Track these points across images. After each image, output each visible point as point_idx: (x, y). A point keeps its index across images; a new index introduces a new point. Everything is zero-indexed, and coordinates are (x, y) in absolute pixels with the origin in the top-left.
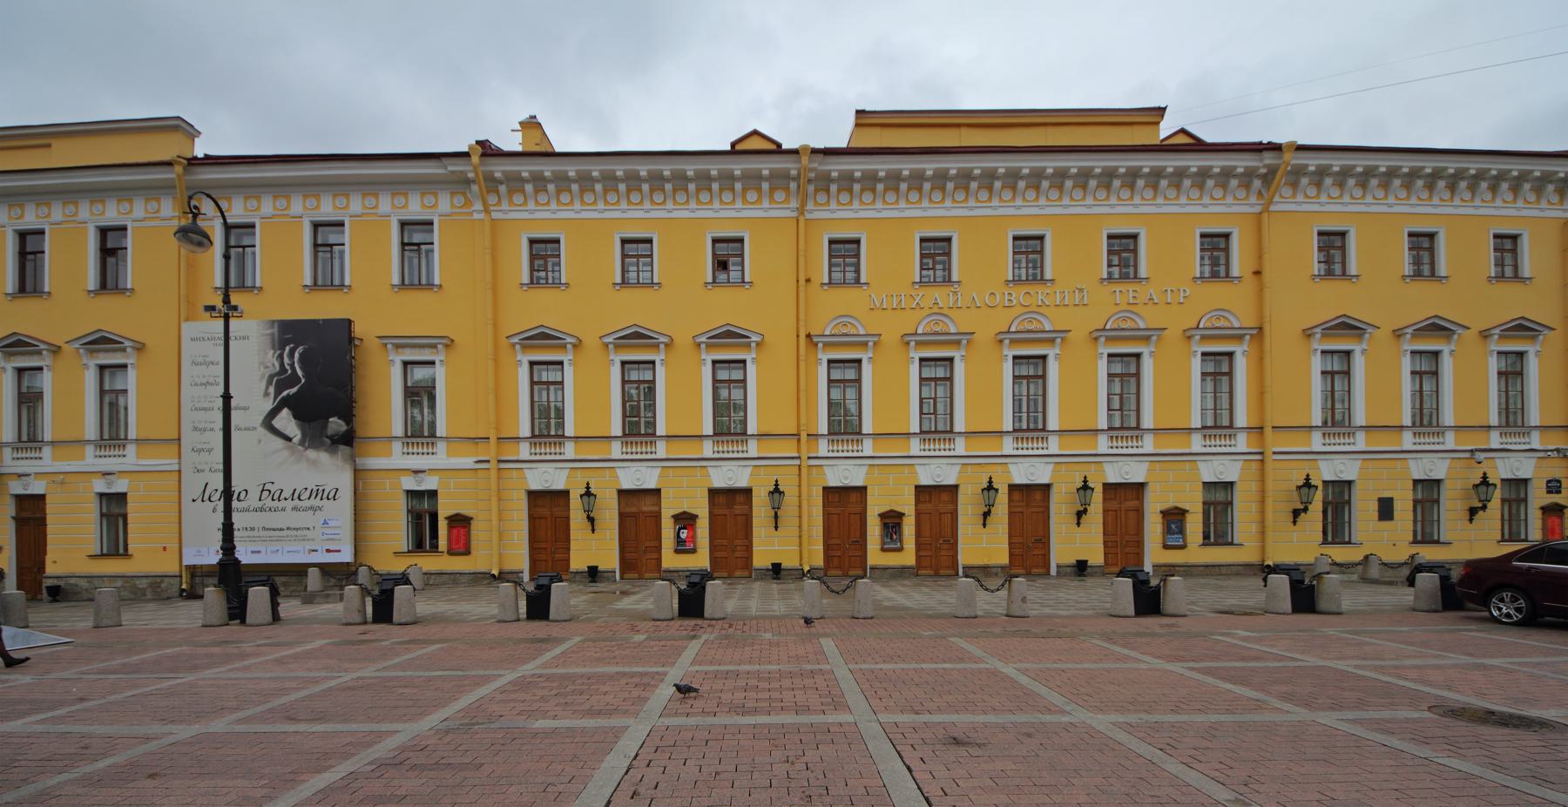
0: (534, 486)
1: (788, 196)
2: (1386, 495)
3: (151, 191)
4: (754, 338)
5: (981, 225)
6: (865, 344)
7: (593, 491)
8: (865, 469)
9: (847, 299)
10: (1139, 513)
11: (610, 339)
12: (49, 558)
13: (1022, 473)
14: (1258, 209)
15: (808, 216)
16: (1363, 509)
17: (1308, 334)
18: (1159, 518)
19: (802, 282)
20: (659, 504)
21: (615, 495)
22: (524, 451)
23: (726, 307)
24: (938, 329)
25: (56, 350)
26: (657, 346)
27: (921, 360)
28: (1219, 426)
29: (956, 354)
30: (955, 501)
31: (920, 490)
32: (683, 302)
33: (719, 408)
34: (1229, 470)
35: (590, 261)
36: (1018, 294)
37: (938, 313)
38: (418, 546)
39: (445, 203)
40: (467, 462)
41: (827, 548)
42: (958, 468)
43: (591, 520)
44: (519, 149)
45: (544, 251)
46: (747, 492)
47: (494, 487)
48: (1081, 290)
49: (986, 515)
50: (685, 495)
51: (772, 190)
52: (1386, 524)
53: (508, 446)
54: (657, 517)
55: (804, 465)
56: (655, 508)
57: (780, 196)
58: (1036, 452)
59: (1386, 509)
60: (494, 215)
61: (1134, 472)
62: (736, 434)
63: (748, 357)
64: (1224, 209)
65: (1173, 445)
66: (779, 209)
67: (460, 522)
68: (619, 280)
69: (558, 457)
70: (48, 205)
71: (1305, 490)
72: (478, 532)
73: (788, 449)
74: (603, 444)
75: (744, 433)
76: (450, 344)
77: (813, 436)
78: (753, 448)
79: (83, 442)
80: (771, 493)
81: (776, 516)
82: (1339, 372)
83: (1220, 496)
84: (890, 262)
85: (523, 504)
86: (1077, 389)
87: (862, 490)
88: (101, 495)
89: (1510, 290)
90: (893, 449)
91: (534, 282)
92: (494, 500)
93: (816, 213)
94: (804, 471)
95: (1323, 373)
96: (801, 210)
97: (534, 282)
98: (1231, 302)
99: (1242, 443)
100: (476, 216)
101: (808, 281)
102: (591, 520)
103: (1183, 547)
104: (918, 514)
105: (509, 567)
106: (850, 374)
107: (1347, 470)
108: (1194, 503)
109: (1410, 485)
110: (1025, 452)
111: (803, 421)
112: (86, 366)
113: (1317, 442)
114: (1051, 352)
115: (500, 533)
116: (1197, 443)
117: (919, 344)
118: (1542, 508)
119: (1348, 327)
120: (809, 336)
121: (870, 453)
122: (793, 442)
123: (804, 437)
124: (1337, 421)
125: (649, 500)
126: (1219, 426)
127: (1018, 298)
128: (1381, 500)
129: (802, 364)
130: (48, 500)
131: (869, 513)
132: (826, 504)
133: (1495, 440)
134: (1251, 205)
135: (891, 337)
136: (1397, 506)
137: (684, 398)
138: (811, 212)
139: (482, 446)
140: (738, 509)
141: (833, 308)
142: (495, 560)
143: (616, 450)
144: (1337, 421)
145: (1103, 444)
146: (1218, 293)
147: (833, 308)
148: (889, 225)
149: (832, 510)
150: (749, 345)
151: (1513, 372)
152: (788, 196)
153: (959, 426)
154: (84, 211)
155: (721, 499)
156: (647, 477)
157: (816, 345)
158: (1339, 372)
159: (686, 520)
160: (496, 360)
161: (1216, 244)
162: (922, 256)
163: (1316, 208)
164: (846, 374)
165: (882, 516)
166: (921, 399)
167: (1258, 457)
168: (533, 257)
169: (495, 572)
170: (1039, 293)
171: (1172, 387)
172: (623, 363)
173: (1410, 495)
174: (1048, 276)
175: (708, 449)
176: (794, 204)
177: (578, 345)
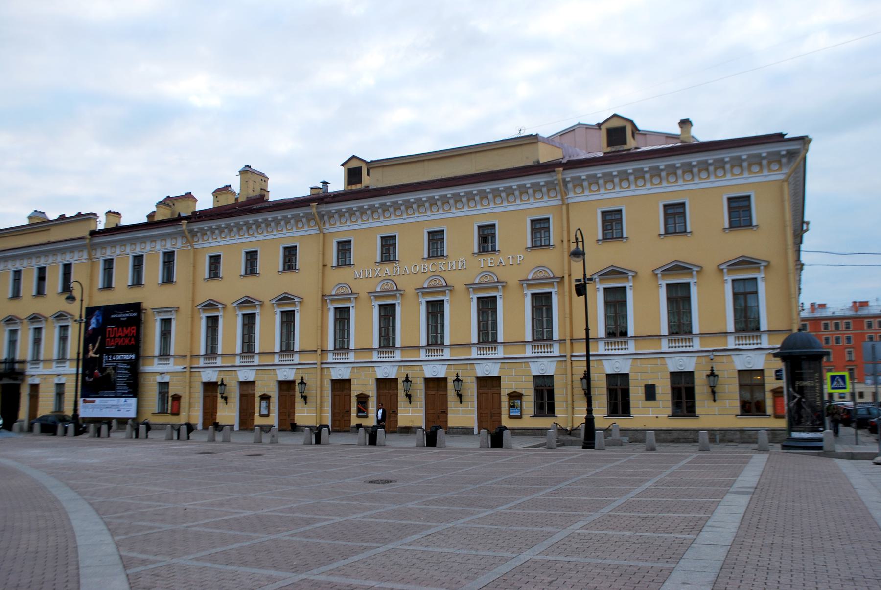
0: (281, 379)
2: (650, 382)
3: (80, 248)
5: (411, 227)
6: (552, 283)
8: (217, 373)
13: (483, 370)
14: (560, 203)
23: (743, 244)
25: (46, 319)
26: (255, 306)
31: (380, 381)
36: (429, 266)
38: (163, 411)
39: (179, 243)
40: (179, 368)
47: (188, 381)
50: (518, 381)
53: (195, 360)
54: (254, 395)
55: (323, 367)
58: (435, 358)
59: (650, 393)
60: (196, 247)
61: (493, 370)
64: (541, 205)
67: (177, 398)
68: (662, 232)
70: (135, 244)
71: (712, 378)
72: (184, 403)
74: (231, 358)
76: (177, 309)
80: (708, 376)
84: (365, 251)
88: (160, 383)
90: (267, 361)
91: (605, 238)
92: (188, 388)
93: (329, 229)
97: (605, 238)
99: (556, 350)
102: (460, 396)
103: (520, 417)
105: (324, 423)
112: (55, 327)
115: (190, 404)
117: (529, 286)
121: (634, 352)
132: (427, 388)
133: (731, 343)
136: (659, 391)
142: (570, 423)
146: (543, 257)
148: (364, 231)
149: (337, 393)
150: (294, 303)
154: (128, 249)
155: (431, 385)
159: (515, 396)
160: (193, 318)
163: (599, 197)
165: (358, 396)
169: (569, 429)
170: (440, 264)
176: (559, 197)
177: (636, 275)
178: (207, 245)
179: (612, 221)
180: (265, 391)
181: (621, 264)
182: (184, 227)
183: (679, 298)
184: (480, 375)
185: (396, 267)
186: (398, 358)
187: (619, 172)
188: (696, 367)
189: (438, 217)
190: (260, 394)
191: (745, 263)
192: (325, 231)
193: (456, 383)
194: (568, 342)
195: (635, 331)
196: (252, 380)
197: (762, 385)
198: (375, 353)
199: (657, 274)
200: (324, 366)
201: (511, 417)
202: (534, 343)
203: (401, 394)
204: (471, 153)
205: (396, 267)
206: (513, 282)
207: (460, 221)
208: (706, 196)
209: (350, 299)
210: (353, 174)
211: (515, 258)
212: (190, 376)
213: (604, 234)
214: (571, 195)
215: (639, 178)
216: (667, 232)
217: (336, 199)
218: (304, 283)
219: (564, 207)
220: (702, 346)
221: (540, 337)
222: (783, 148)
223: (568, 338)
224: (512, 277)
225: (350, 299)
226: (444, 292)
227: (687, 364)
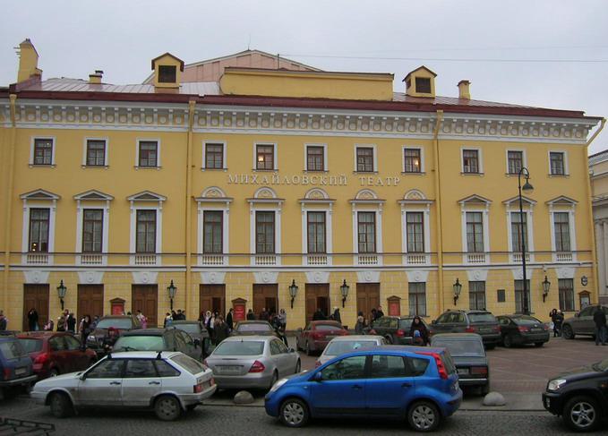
1: (21, 117)
4: (161, 199)
5: (291, 139)
7: (64, 285)
8: (379, 273)
9: (214, 177)
10: (378, 298)
11: (24, 197)
13: (363, 277)
14: (433, 137)
15: (194, 131)
16: (491, 296)
17: (459, 203)
18: (110, 304)
19: (190, 167)
23: (147, 181)
27: (407, 213)
28: (416, 251)
29: (377, 211)
32: (121, 178)
33: (87, 236)
34: (422, 276)
35: (70, 153)
36: (310, 177)
37: (266, 187)
42: (102, 274)
44: (217, 94)
45: (43, 148)
46: (155, 286)
48: (343, 177)
49: (545, 296)
50: (118, 289)
51: (174, 117)
52: (502, 304)
57: (178, 120)
59: (501, 296)
61: (373, 277)
64: (415, 137)
66: (178, 128)
68: (32, 162)
69: (43, 265)
71: (172, 290)
73: (179, 262)
77: (195, 255)
79: (301, 255)
81: (62, 302)
82: (475, 225)
83: (567, 285)
85: (21, 292)
86: (342, 232)
89: (558, 181)
93: (197, 129)
95: (467, 223)
96: (191, 128)
98: (420, 186)
99: (428, 261)
100: (6, 126)
101: (193, 166)
106: (319, 219)
107: (481, 275)
109: (407, 285)
110: (414, 265)
111: (189, 246)
113: (465, 261)
114: (328, 210)
116: (405, 262)
118: (111, 301)
119: (477, 200)
120: (193, 197)
121: (228, 265)
122: (182, 258)
123: (189, 255)
124: (475, 249)
126: (416, 251)
128: (498, 291)
129: (189, 216)
131: (381, 297)
134: (429, 136)
135: (391, 201)
136: (495, 295)
137: (119, 230)
138: (196, 129)
140: (149, 297)
141: (209, 183)
143: (78, 261)
144: (475, 249)
145: (356, 262)
146: (414, 180)
147: (209, 183)
151: (562, 224)
152: (21, 117)
153: (379, 250)
156: (94, 277)
157: (197, 202)
158: (475, 225)
161: (412, 154)
162: (358, 156)
164: (214, 221)
167: (590, 265)
168: (36, 148)
170: (321, 177)
171: (391, 231)
172: (84, 210)
173: (513, 288)
174: (481, 171)
175: (132, 261)
178: (204, 131)
179: (43, 149)
180: (117, 295)
181: (152, 189)
182: (13, 102)
183: (317, 223)
184: (83, 282)
185: (275, 176)
186: (278, 265)
187: (41, 107)
189: (332, 134)
190: (386, 297)
191: (94, 196)
192: (439, 138)
194: (440, 254)
195: (577, 245)
204: (278, 76)
205: (275, 176)
206: (391, 201)
207: (341, 141)
208: (493, 144)
209: (378, 204)
210: (167, 71)
211: (389, 177)
213: (88, 161)
214: (195, 126)
215: (253, 119)
216: (35, 163)
217: (94, 97)
218: (166, 180)
219: (436, 142)
220: (162, 262)
221: (89, 249)
222: (577, 123)
224: (342, 196)
225: (278, 203)
226: (378, 204)
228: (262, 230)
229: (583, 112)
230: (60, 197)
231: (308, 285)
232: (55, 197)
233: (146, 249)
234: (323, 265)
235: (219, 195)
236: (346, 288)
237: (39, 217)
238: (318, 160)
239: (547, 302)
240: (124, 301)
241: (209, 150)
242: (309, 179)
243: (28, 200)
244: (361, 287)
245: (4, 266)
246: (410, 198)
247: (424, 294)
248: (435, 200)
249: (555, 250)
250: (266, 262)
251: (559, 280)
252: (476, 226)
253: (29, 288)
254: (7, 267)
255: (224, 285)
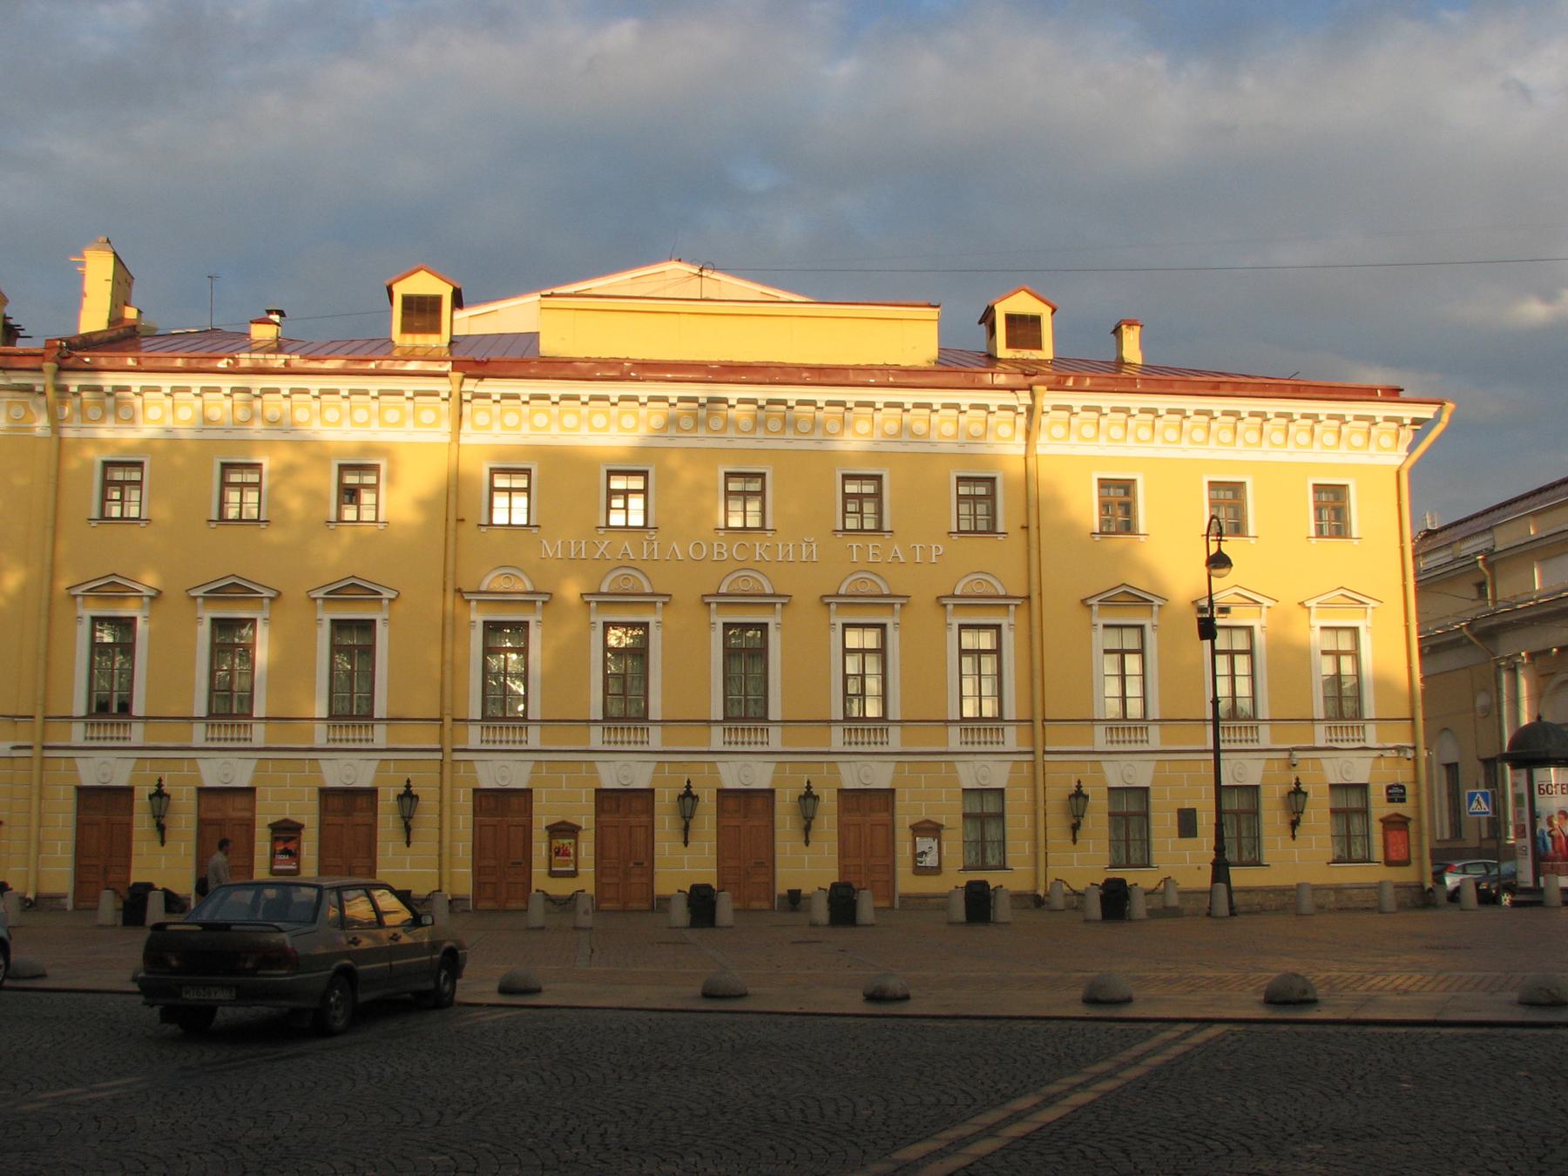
11: (78, 591)
12: (135, 863)
13: (736, 774)
16: (1163, 822)
20: (252, 809)
21: (194, 795)
22: (78, 733)
24: (629, 587)
30: (650, 810)
31: (327, 795)
34: (996, 774)
41: (478, 871)
42: (1008, 766)
43: (161, 828)
46: (372, 793)
54: (249, 825)
55: (447, 756)
56: (247, 814)
59: (1187, 823)
61: (879, 775)
62: (358, 717)
63: (379, 617)
65: (925, 741)
69: (364, 745)
73: (425, 737)
74: (181, 727)
75: (370, 716)
78: (380, 735)
80: (400, 797)
87: (526, 793)
90: (170, 735)
94: (447, 768)
99: (1012, 738)
102: (161, 828)
104: (323, 826)
105: (50, 888)
108: (950, 814)
115: (39, 843)
120: (459, 591)
122: (434, 729)
123: (448, 720)
125: (240, 802)
127: (729, 550)
130: (1152, 793)
131: (898, 824)
132: (721, 810)
133: (1320, 736)
136: (1171, 820)
139: (23, 726)
143: (199, 734)
156: (240, 772)
166: (606, 677)
167: (1029, 757)
169: (31, 895)
179: (121, 485)
180: (288, 812)
185: (650, 542)
188: (1264, 777)
193: (156, 799)
196: (244, 782)
197: (1364, 812)
198: (717, 733)
199: (945, 605)
200: (458, 756)
201: (553, 874)
202: (727, 725)
203: (142, 822)
205: (650, 542)
212: (42, 769)
220: (543, 741)
223: (1039, 718)
227: (756, 774)
228: (738, 667)
229: (534, 337)
230: (279, 593)
231: (723, 794)
232: (266, 594)
233: (352, 707)
234: (759, 748)
235: (992, 592)
236: (810, 801)
237: (229, 637)
238: (981, 509)
239: (167, 843)
240: (579, 828)
241: (732, 487)
242: (729, 550)
243: (205, 598)
244: (852, 799)
245: (30, 747)
246: (968, 591)
247: (1000, 816)
248: (1028, 598)
249: (1322, 716)
250: (748, 739)
251: (1332, 786)
252: (1237, 657)
253: (88, 796)
254: (38, 749)
255: (530, 791)
